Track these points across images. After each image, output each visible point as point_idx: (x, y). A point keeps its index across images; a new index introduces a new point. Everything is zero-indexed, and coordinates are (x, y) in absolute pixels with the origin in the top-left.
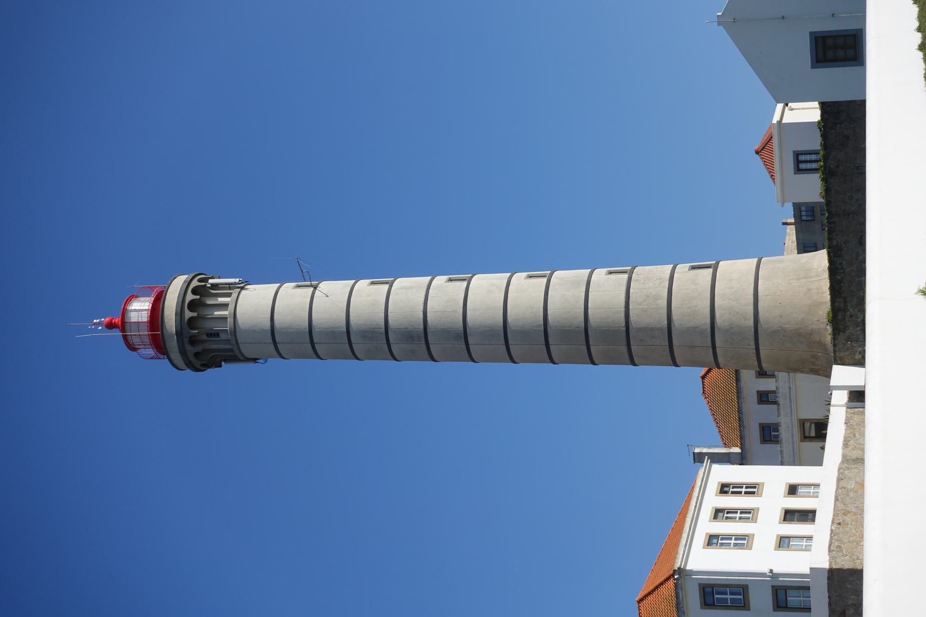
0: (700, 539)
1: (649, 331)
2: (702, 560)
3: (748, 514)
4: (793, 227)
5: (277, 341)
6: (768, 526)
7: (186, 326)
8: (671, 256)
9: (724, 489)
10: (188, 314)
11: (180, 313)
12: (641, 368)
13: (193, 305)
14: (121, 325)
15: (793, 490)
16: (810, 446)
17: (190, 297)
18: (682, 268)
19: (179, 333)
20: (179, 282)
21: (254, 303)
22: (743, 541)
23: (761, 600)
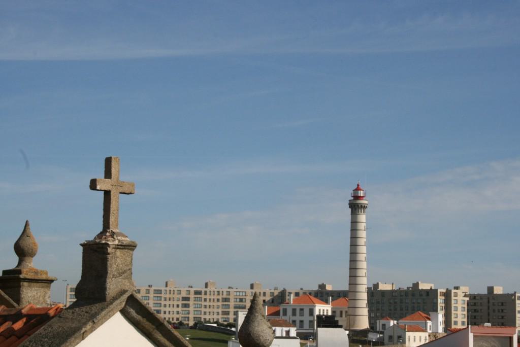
0: (320, 308)
5: (354, 223)
10: (360, 205)
11: (363, 204)
13: (362, 206)
14: (358, 189)
17: (363, 205)
20: (366, 202)
21: (362, 218)
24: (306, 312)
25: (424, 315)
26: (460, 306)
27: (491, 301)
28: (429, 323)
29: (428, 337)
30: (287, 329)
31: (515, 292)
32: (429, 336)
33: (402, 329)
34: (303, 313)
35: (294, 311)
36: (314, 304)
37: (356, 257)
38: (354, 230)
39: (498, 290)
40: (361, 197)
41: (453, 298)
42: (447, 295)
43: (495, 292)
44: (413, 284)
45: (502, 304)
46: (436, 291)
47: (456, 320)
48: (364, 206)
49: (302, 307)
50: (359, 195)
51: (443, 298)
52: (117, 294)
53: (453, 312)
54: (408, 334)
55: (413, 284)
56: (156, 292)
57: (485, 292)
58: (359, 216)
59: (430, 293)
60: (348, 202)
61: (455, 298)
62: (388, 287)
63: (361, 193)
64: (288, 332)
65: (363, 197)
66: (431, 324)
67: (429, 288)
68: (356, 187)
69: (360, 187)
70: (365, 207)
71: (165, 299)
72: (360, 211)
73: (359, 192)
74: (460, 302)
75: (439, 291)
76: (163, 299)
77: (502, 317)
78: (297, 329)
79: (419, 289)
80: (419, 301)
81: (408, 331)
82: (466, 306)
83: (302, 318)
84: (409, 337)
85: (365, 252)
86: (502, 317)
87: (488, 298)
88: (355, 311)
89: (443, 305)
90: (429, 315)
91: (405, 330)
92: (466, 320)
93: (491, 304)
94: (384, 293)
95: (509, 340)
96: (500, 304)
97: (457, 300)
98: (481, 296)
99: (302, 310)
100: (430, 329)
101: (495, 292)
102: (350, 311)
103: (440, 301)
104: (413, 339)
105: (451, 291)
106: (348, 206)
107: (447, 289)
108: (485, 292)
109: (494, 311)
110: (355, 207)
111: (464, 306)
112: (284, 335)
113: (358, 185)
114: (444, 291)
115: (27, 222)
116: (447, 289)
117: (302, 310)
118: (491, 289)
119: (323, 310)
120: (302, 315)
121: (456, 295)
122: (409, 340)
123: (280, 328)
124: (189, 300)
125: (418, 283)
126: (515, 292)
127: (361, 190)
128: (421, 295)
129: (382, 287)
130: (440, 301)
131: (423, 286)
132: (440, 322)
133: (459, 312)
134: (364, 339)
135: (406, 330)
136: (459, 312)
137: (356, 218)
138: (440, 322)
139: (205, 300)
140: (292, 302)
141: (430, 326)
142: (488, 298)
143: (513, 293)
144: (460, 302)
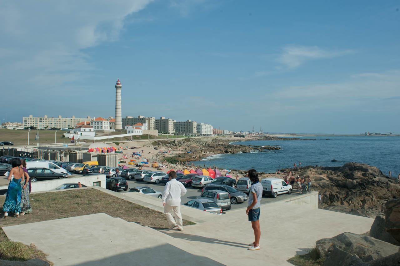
14: (118, 81)
23: (101, 126)
26: (152, 123)
27: (161, 121)
30: (84, 128)
39: (163, 118)
43: (163, 119)
44: (138, 116)
46: (145, 118)
55: (138, 116)
56: (111, 134)
57: (160, 119)
62: (131, 117)
63: (119, 83)
64: (90, 130)
71: (58, 122)
74: (152, 122)
75: (146, 118)
76: (28, 123)
83: (98, 126)
92: (154, 127)
94: (129, 119)
98: (136, 119)
101: (163, 119)
108: (160, 119)
110: (117, 87)
112: (89, 131)
115: (188, 198)
120: (98, 124)
121: (151, 119)
123: (88, 128)
124: (97, 129)
125: (127, 117)
129: (129, 117)
130: (147, 121)
139: (72, 122)
144: (152, 122)
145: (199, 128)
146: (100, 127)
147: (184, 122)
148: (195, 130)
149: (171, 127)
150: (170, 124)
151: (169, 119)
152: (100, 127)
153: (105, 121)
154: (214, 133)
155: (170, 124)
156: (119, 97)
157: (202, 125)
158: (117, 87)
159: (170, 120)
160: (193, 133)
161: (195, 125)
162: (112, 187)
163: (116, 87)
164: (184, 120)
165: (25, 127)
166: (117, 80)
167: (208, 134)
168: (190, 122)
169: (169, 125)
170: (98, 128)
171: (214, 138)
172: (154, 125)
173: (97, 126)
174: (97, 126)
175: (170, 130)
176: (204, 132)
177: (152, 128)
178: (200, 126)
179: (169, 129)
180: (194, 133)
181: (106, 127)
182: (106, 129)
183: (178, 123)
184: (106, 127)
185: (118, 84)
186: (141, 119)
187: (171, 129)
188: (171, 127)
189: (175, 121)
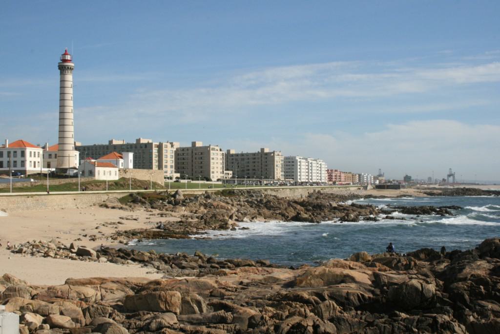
0: (31, 150)
1: (64, 122)
2: (28, 150)
3: (35, 156)
4: (72, 89)
5: (63, 81)
6: (33, 159)
7: (65, 66)
8: (74, 106)
9: (39, 153)
10: (67, 67)
11: (67, 66)
12: (59, 101)
13: (68, 68)
14: (66, 54)
15: (39, 162)
16: (46, 165)
17: (69, 67)
18: (73, 121)
19: (64, 66)
20: (73, 65)
21: (69, 77)
22: (31, 156)
23: (23, 159)
24: (19, 153)
25: (118, 155)
27: (194, 152)
28: (121, 161)
29: (118, 172)
31: (210, 145)
32: (119, 171)
33: (92, 165)
34: (16, 155)
35: (9, 153)
36: (25, 147)
37: (64, 109)
38: (63, 87)
39: (199, 144)
40: (68, 60)
41: (164, 149)
42: (160, 147)
45: (202, 154)
46: (152, 144)
47: (166, 164)
48: (71, 68)
49: (15, 150)
50: (66, 59)
51: (157, 149)
52: (130, 231)
53: (164, 159)
54: (97, 169)
57: (190, 145)
58: (66, 76)
59: (147, 146)
60: (58, 65)
61: (166, 149)
62: (120, 142)
63: (68, 57)
65: (70, 60)
66: (123, 162)
67: (147, 142)
68: (64, 52)
69: (68, 52)
70: (71, 69)
72: (67, 71)
73: (67, 56)
77: (201, 163)
78: (433, 293)
79: (140, 143)
80: (140, 151)
81: (97, 167)
82: (173, 154)
83: (15, 159)
84: (99, 171)
85: (72, 105)
86: (201, 163)
87: (192, 150)
88: (63, 153)
89: (157, 154)
90: (122, 154)
91: (95, 165)
92: (173, 164)
93: (194, 154)
95: (61, 139)
96: (200, 154)
97: (167, 150)
98: (188, 149)
99: (15, 152)
100: (122, 166)
102: (59, 154)
103: (155, 151)
104: (114, 174)
105: (162, 144)
106: (58, 68)
107: (160, 143)
109: (196, 158)
110: (63, 69)
111: (172, 154)
113: (66, 51)
114: (158, 144)
116: (160, 143)
117: (15, 152)
118: (194, 144)
119: (35, 152)
120: (15, 156)
122: (99, 174)
126: (210, 145)
127: (68, 54)
128: (141, 147)
129: (115, 142)
130: (155, 151)
131: (144, 141)
132: (131, 160)
133: (169, 159)
134: (64, 174)
135: (96, 165)
136: (169, 159)
137: (64, 78)
138: (131, 160)
140: (7, 146)
141: (122, 163)
142: (192, 150)
143: (208, 145)
145: (290, 165)
146: (19, 164)
147: (254, 154)
148: (279, 173)
149: (215, 166)
150: (213, 159)
151: (211, 147)
152: (19, 164)
153: (33, 150)
154: (330, 179)
155: (213, 159)
156: (70, 91)
157: (299, 160)
158: (63, 69)
159: (213, 149)
160: (274, 178)
161: (278, 161)
162: (425, 253)
163: (59, 69)
164: (252, 148)
165: (168, 181)
166: (64, 52)
167: (314, 181)
168: (266, 154)
169: (212, 161)
170: (15, 166)
171: (314, 191)
172: (173, 159)
173: (12, 159)
174: (12, 159)
175: (213, 172)
176: (302, 177)
177: (169, 167)
178: (293, 162)
179: (212, 170)
180: (276, 178)
181: (35, 162)
182: (35, 167)
183: (240, 157)
184: (35, 162)
185: (65, 61)
186: (144, 147)
187: (217, 170)
188: (215, 166)
189: (177, 145)
